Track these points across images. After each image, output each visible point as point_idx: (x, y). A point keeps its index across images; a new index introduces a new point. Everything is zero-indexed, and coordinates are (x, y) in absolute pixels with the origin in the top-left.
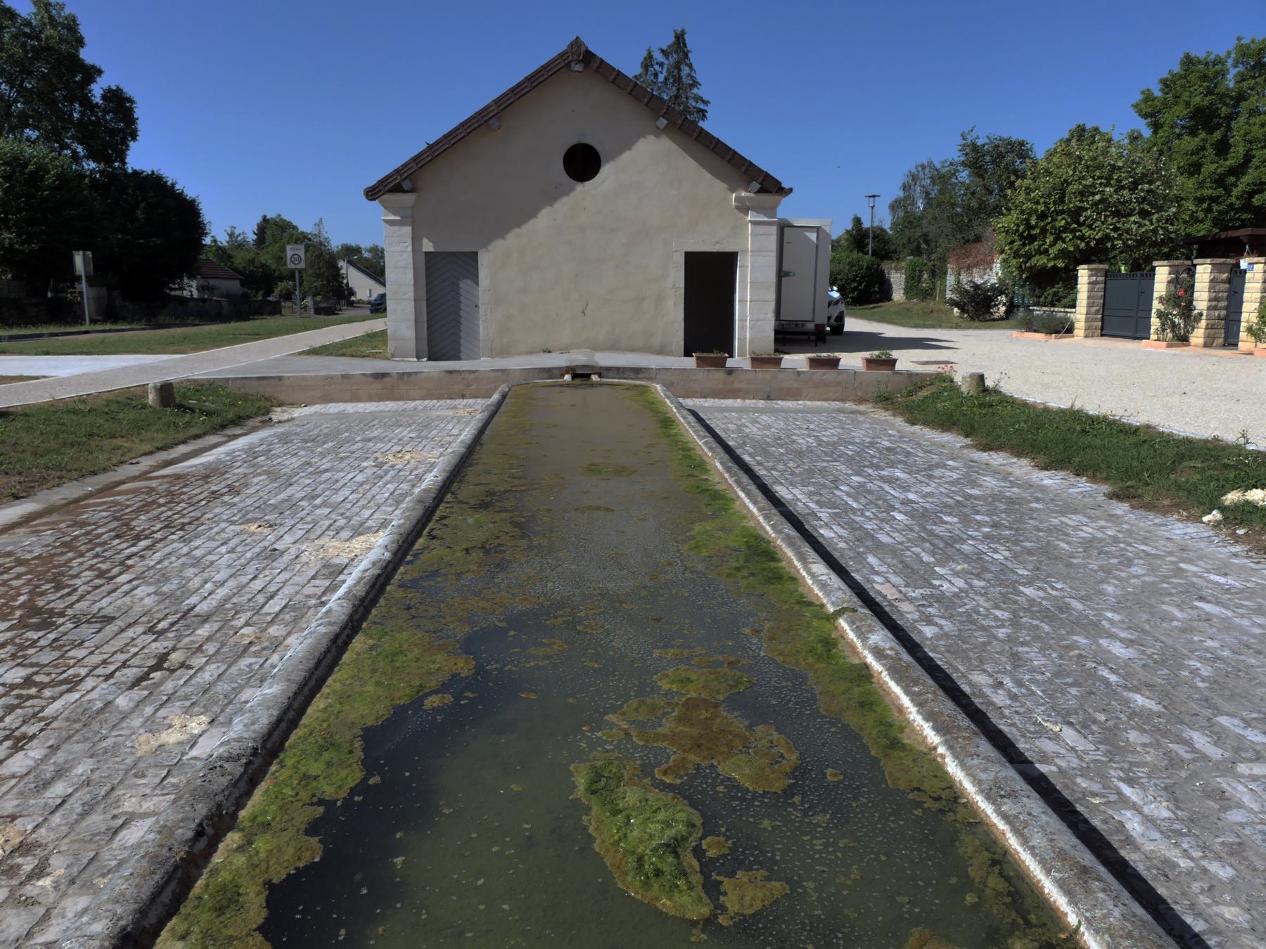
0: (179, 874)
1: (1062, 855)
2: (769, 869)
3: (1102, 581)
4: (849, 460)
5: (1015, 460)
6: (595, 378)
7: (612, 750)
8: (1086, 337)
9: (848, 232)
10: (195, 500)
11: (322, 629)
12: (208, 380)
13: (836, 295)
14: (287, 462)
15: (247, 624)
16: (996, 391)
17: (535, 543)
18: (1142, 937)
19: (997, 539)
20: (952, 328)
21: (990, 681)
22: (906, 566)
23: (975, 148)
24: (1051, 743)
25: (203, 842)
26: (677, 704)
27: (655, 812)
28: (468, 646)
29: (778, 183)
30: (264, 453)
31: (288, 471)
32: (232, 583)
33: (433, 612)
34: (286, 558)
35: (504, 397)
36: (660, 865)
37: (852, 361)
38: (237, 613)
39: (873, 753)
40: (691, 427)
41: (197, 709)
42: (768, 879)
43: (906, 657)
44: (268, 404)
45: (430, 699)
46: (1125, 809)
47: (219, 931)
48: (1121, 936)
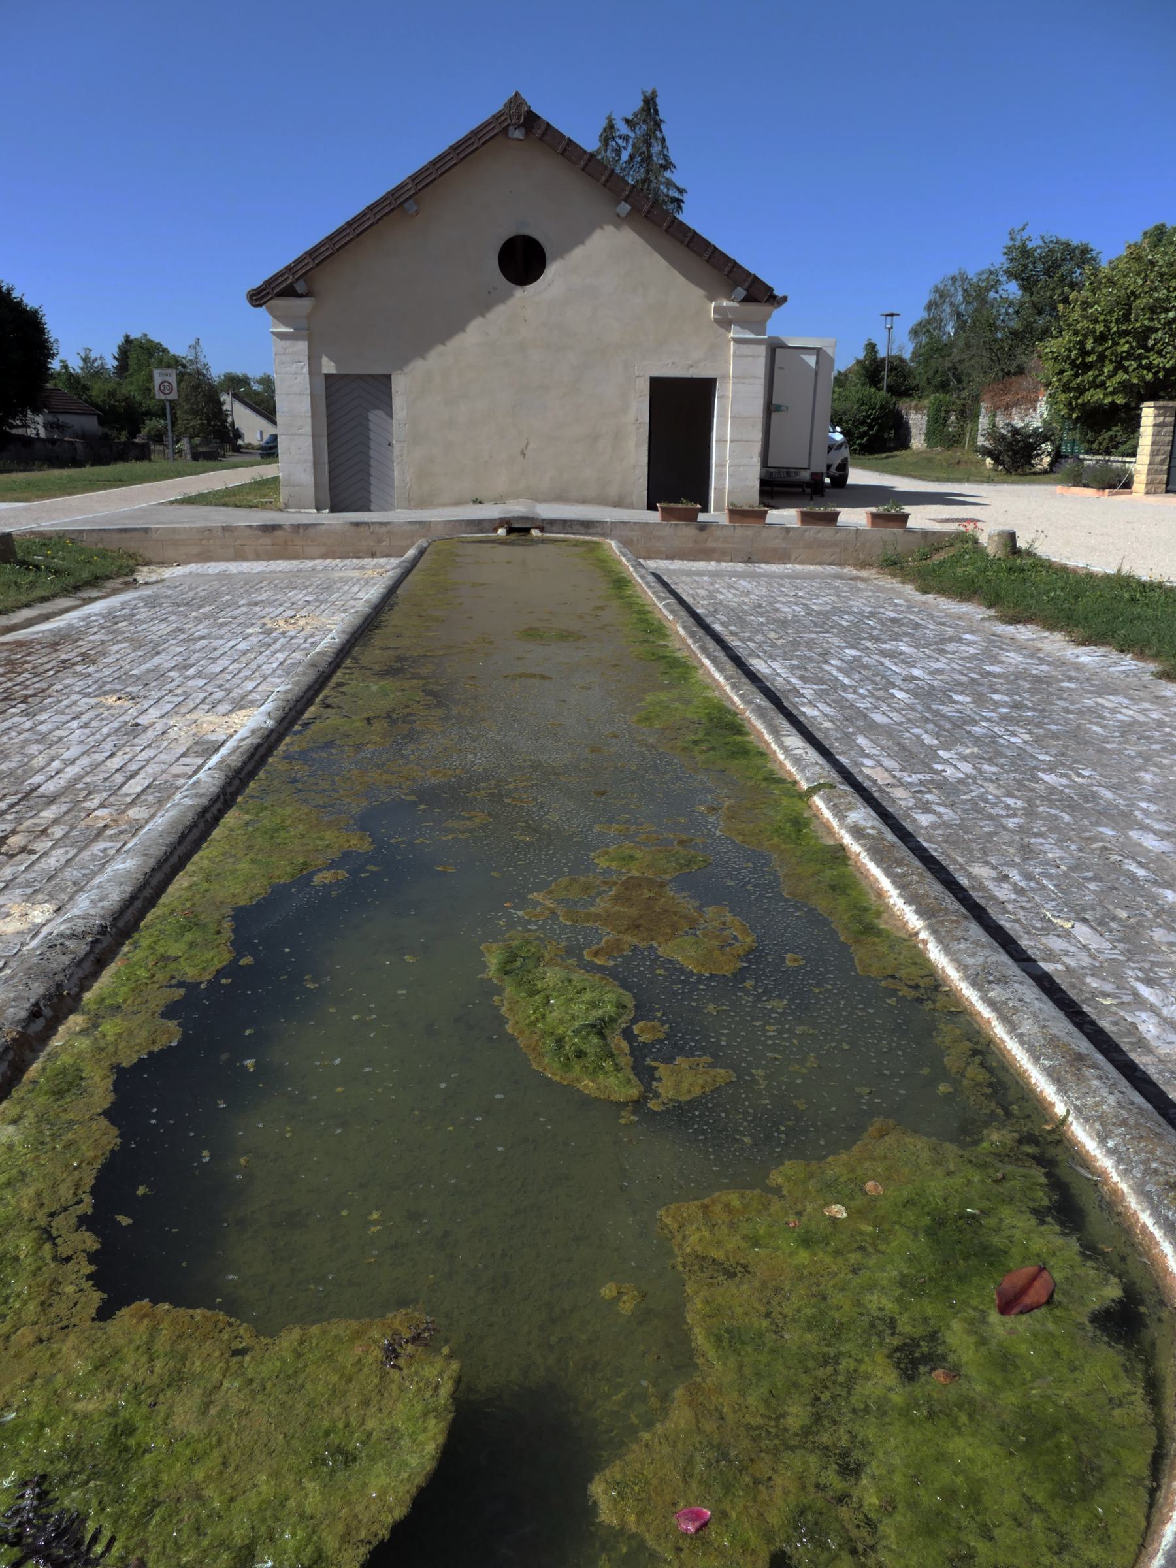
0: (11, 1056)
1: (1054, 1042)
2: (715, 1056)
3: (1140, 769)
4: (844, 632)
5: (1047, 634)
6: (535, 533)
7: (536, 931)
8: (1147, 493)
9: (859, 362)
10: (41, 670)
11: (188, 801)
12: (57, 532)
13: (838, 437)
14: (155, 629)
15: (102, 806)
16: (1029, 553)
17: (454, 712)
18: (1137, 1125)
19: (1017, 722)
20: (982, 482)
21: (994, 874)
22: (903, 748)
23: (1025, 252)
24: (1059, 941)
25: (39, 1024)
26: (615, 883)
27: (579, 992)
28: (365, 823)
29: (770, 289)
30: (125, 618)
31: (155, 637)
32: (85, 761)
33: (324, 785)
34: (151, 734)
35: (422, 552)
36: (582, 1047)
37: (854, 517)
38: (89, 794)
39: (842, 939)
40: (650, 587)
41: (40, 897)
42: (712, 1066)
43: (890, 836)
44: (132, 562)
45: (321, 875)
46: (1141, 1010)
47: (57, 1116)
48: (1114, 1124)
